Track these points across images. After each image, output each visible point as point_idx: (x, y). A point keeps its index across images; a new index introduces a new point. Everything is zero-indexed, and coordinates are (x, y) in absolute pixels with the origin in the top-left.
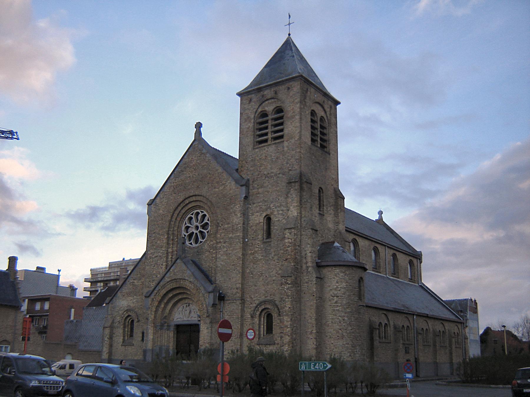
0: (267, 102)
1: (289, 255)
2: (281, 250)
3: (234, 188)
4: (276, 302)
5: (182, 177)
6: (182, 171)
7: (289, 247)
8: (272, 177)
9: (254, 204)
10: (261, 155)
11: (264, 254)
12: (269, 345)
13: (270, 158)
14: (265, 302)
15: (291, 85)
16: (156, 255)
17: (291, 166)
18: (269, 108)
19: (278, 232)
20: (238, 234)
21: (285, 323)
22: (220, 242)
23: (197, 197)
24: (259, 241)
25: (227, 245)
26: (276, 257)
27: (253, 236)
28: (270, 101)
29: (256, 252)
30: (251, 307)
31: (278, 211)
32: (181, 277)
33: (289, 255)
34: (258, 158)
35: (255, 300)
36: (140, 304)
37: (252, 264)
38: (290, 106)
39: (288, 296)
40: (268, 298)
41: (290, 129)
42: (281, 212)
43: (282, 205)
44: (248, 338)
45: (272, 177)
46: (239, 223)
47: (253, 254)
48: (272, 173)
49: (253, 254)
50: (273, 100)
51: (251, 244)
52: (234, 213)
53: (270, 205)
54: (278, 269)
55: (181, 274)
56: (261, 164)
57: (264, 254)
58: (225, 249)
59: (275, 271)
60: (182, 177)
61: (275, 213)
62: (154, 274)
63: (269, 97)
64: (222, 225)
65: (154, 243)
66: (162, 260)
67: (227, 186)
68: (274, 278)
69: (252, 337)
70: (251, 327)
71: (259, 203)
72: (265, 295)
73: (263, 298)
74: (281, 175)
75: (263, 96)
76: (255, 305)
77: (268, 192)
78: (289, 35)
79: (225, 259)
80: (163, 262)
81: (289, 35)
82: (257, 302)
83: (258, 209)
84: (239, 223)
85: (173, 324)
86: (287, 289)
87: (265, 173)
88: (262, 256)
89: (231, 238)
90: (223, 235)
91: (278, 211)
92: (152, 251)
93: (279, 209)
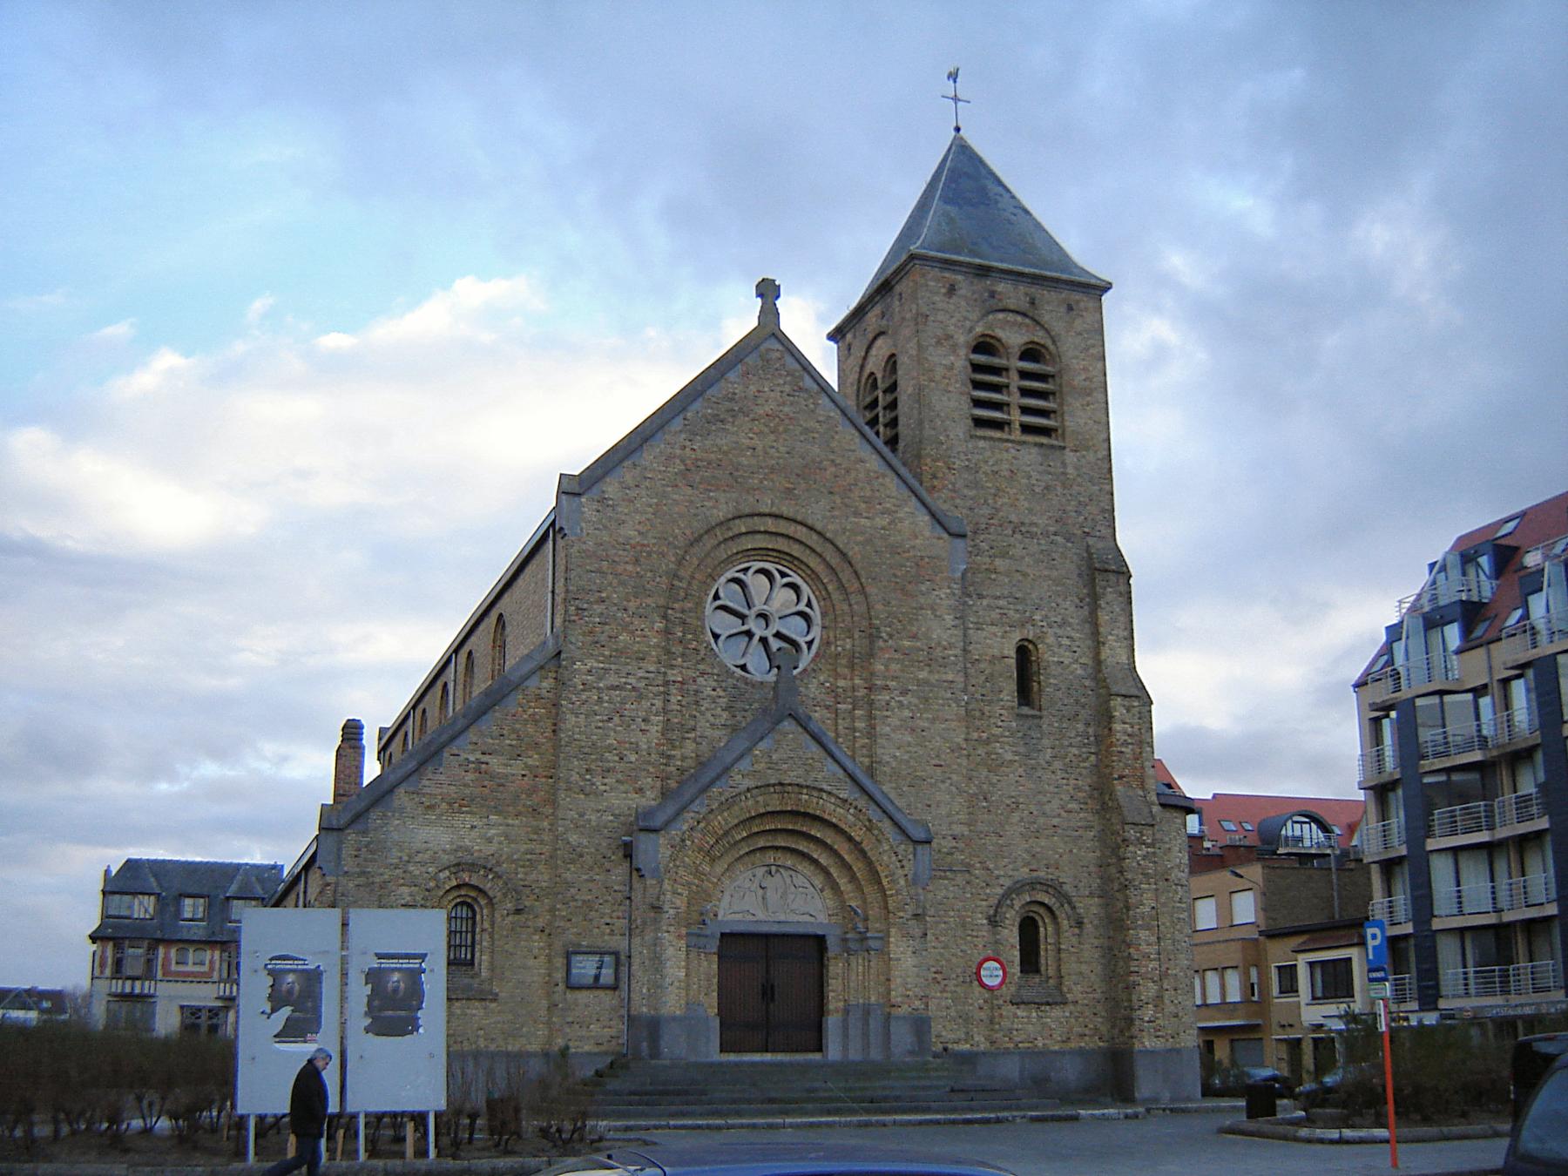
0: (1001, 316)
1: (1127, 765)
2: (1071, 745)
3: (927, 534)
4: (1065, 887)
5: (724, 442)
6: (717, 419)
7: (1125, 744)
8: (1032, 536)
9: (981, 597)
10: (996, 463)
11: (1022, 750)
12: (1048, 1004)
13: (1024, 481)
14: (1033, 884)
15: (1078, 302)
16: (612, 680)
17: (1090, 523)
18: (1014, 337)
19: (1059, 694)
20: (950, 677)
21: (1143, 947)
22: (886, 688)
23: (782, 522)
24: (1003, 708)
25: (915, 701)
26: (1057, 764)
27: (981, 691)
28: (1011, 317)
29: (997, 739)
30: (988, 895)
31: (1058, 637)
32: (800, 781)
33: (1127, 765)
34: (986, 468)
35: (998, 877)
36: (523, 848)
37: (985, 773)
38: (988, 331)
39: (1145, 875)
40: (1042, 874)
41: (1082, 422)
42: (1066, 642)
43: (1070, 625)
44: (983, 985)
45: (1032, 536)
46: (951, 646)
47: (987, 742)
48: (1033, 524)
49: (987, 742)
50: (1019, 318)
51: (978, 714)
52: (933, 609)
53: (1032, 613)
54: (1066, 798)
55: (801, 772)
56: (998, 489)
57: (1022, 750)
58: (907, 713)
59: (1056, 803)
60: (724, 442)
61: (1050, 640)
62: (610, 749)
63: (1011, 303)
64: (891, 636)
65: (603, 638)
66: (645, 704)
67: (901, 520)
68: (1055, 821)
69: (997, 981)
70: (990, 953)
71: (998, 598)
72: (1029, 863)
73: (1024, 873)
74: (1059, 539)
75: (992, 294)
76: (1000, 891)
77: (1025, 575)
78: (958, 129)
79: (909, 744)
80: (649, 711)
81: (958, 129)
82: (1008, 883)
83: (995, 615)
84: (951, 646)
85: (714, 930)
86: (1144, 857)
87: (1013, 518)
88: (1016, 753)
89: (926, 682)
90: (894, 666)
91: (1058, 637)
92: (592, 663)
93: (1060, 632)
